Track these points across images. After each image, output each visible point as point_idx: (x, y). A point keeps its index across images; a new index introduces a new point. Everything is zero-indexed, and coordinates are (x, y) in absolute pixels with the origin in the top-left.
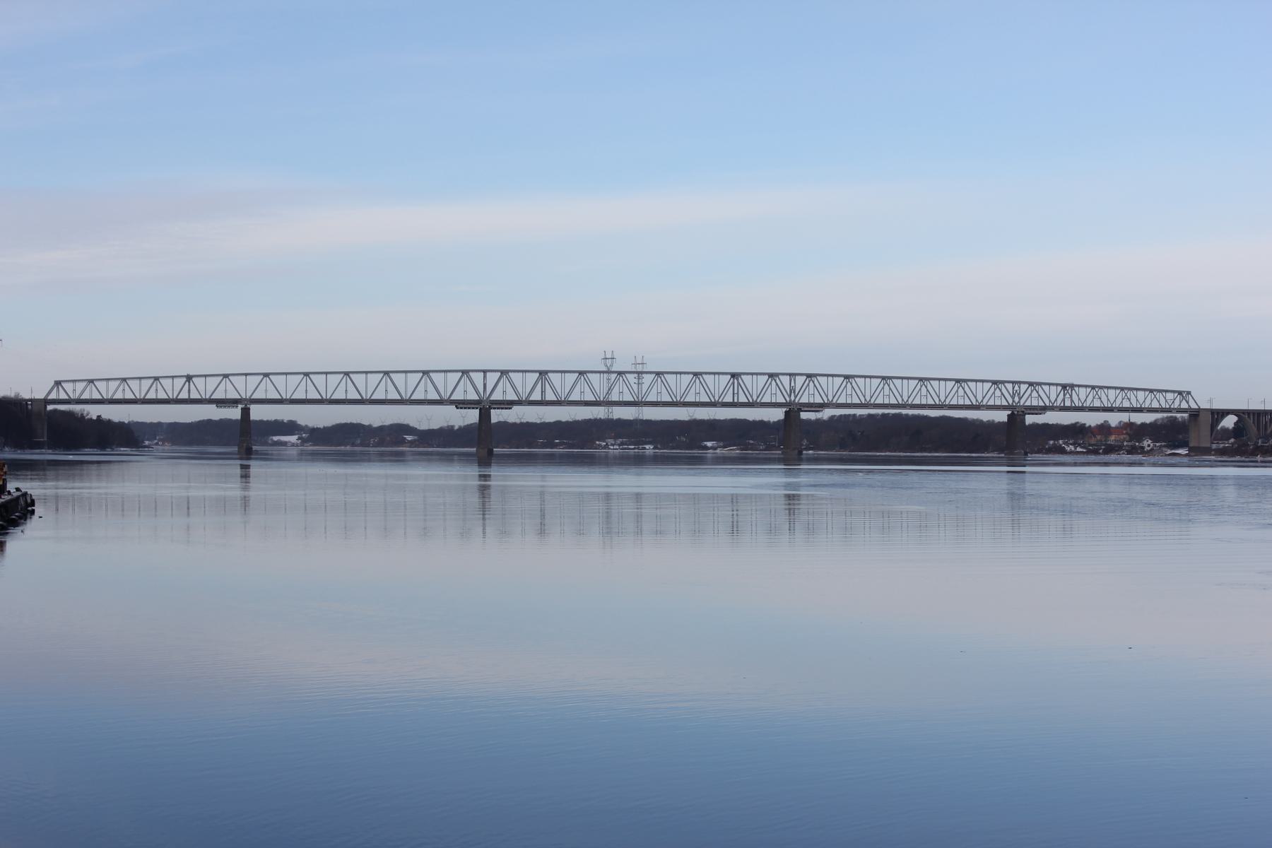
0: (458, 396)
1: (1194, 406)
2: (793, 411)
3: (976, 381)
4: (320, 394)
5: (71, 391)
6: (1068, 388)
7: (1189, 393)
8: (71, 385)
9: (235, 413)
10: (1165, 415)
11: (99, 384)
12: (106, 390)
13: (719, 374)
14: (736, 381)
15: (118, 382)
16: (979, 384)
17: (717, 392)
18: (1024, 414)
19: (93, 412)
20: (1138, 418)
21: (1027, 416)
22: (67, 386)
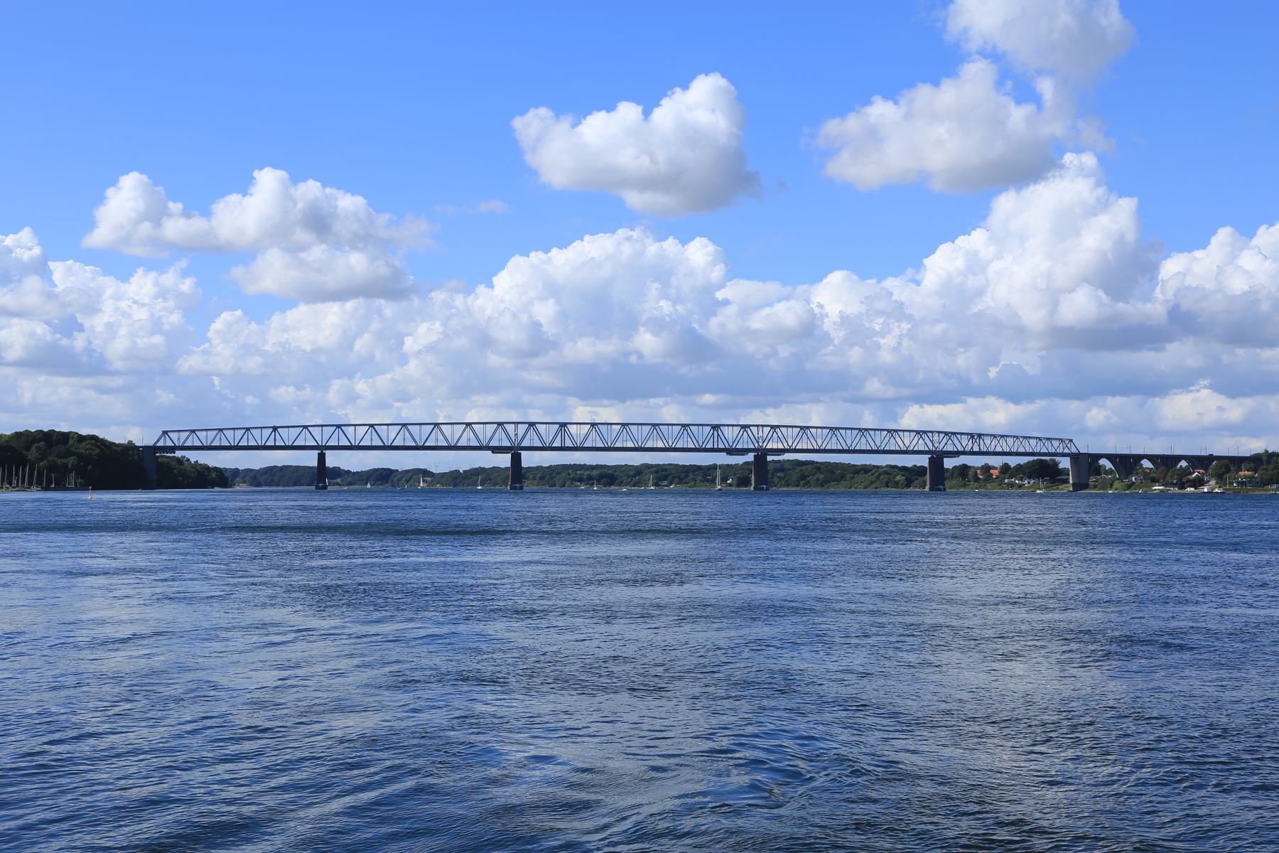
0: (494, 443)
1: (1074, 450)
2: (761, 454)
3: (846, 429)
4: (173, 442)
5: (177, 439)
6: (976, 437)
7: (1071, 441)
8: (176, 434)
9: (504, 460)
10: (1035, 458)
11: (350, 430)
12: (206, 438)
13: (641, 424)
14: (715, 432)
15: (216, 432)
16: (790, 429)
17: (609, 439)
18: (766, 455)
19: (193, 456)
20: (1013, 461)
21: (945, 459)
22: (573, 429)
